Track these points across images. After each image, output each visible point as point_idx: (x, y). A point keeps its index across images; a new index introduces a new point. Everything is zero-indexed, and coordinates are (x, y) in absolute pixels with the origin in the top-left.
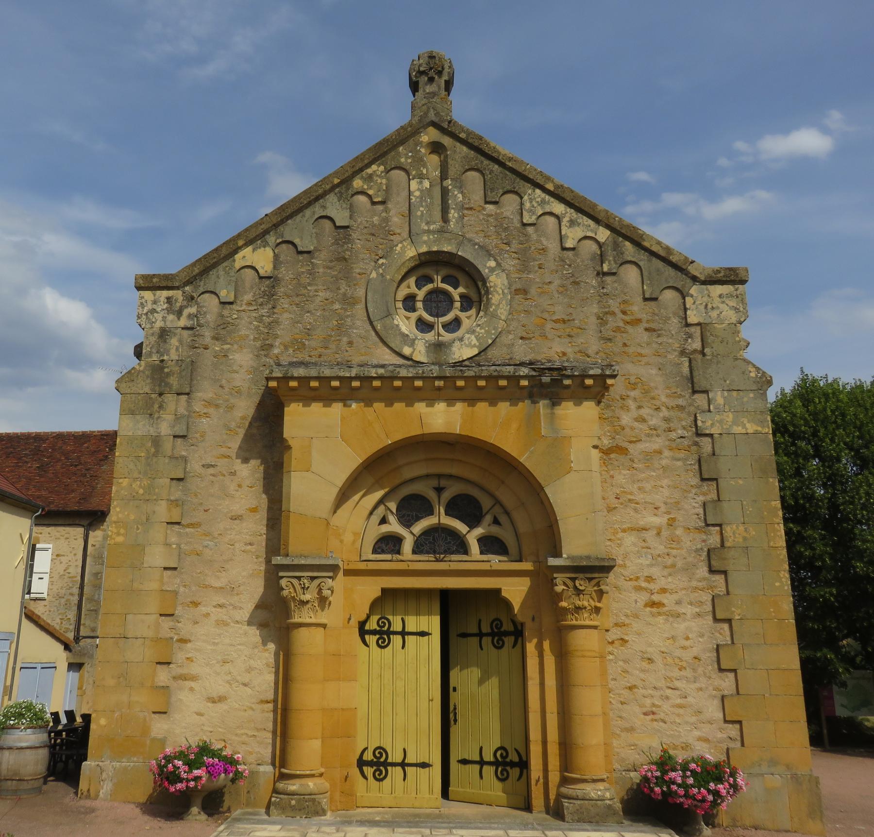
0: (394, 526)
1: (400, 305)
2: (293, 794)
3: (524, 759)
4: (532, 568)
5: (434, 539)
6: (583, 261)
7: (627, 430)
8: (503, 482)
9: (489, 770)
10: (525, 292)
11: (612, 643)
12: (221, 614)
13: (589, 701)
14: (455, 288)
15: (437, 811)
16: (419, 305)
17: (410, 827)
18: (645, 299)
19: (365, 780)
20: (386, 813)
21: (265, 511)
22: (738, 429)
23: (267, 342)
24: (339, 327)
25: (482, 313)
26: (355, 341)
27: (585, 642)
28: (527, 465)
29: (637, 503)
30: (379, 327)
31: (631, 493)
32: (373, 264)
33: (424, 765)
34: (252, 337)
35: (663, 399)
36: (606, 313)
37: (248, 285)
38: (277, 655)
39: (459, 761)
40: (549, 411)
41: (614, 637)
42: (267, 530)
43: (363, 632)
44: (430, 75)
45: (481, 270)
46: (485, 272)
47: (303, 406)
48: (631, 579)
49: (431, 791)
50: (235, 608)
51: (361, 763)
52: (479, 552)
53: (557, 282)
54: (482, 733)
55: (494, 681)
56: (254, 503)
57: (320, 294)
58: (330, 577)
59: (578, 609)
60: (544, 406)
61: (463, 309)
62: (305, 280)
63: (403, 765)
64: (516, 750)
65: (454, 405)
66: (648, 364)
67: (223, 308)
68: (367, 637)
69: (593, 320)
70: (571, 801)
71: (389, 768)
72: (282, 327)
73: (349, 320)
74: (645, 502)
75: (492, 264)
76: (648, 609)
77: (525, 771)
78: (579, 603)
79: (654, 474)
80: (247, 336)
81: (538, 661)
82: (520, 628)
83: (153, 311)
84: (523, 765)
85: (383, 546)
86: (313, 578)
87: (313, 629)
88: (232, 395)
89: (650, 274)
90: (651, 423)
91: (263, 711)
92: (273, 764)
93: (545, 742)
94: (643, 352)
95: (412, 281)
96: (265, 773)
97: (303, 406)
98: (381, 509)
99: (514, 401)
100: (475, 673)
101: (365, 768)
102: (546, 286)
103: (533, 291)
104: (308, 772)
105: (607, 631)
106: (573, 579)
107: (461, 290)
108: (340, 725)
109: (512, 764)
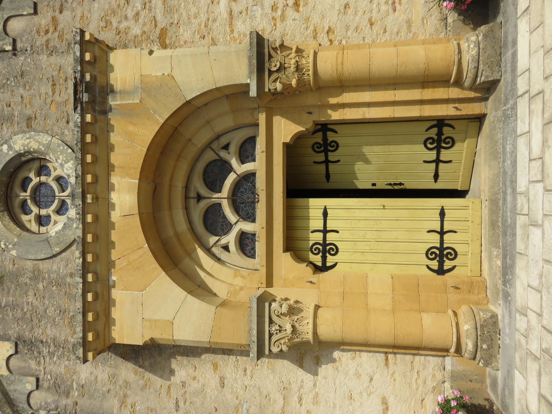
0: (231, 239)
1: (43, 229)
2: (476, 346)
3: (435, 123)
4: (264, 114)
5: (242, 203)
6: (4, 68)
7: (145, 29)
8: (190, 140)
9: (445, 155)
10: (29, 119)
11: (331, 41)
12: (308, 399)
13: (384, 58)
14: (31, 180)
15: (486, 204)
17: (514, 235)
18: (36, 12)
19: (456, 268)
20: (490, 253)
21: (216, 356)
23: (71, 349)
24: (58, 285)
25: (48, 158)
26: (70, 271)
27: (328, 64)
28: (166, 116)
29: (208, 19)
30: (57, 250)
31: (200, 25)
32: (6, 253)
33: (442, 214)
34: (67, 362)
36: (47, 47)
37: (23, 364)
38: (343, 351)
39: (436, 181)
40: (118, 95)
41: (326, 39)
42: (233, 355)
43: (324, 268)
45: (10, 158)
46: (12, 154)
47: (115, 325)
48: (275, 25)
49: (466, 208)
50: (302, 387)
51: (441, 271)
52: (253, 163)
53: (21, 91)
54: (410, 161)
55: (366, 150)
56: (209, 366)
57: (30, 300)
58: (270, 305)
59: (298, 68)
60: (115, 101)
61: (48, 174)
62: (19, 314)
63: (442, 233)
64: (426, 131)
65: (113, 185)
66: (90, 11)
67: (42, 387)
68: (328, 264)
69: (53, 59)
70: (479, 74)
71: (445, 246)
72: (58, 336)
73: (52, 276)
74: (207, 12)
75: (5, 147)
76: (301, 9)
77: (446, 122)
78: (293, 69)
79: (183, 4)
80: (66, 366)
81: (348, 107)
82: (319, 127)
84: (440, 123)
85: (248, 248)
86: (271, 322)
87: (319, 321)
88: (115, 383)
89: (14, 9)
90: (139, 8)
91: (395, 363)
92: (444, 356)
93: (422, 102)
94: (79, 15)
95: (25, 218)
96: (452, 365)
97: (115, 325)
98: (215, 250)
99: (108, 129)
100: (359, 167)
101: (445, 268)
102: (25, 101)
103: (28, 112)
104: (455, 330)
105: (320, 45)
106: (271, 73)
107: (32, 175)
108: (408, 293)
109: (440, 133)
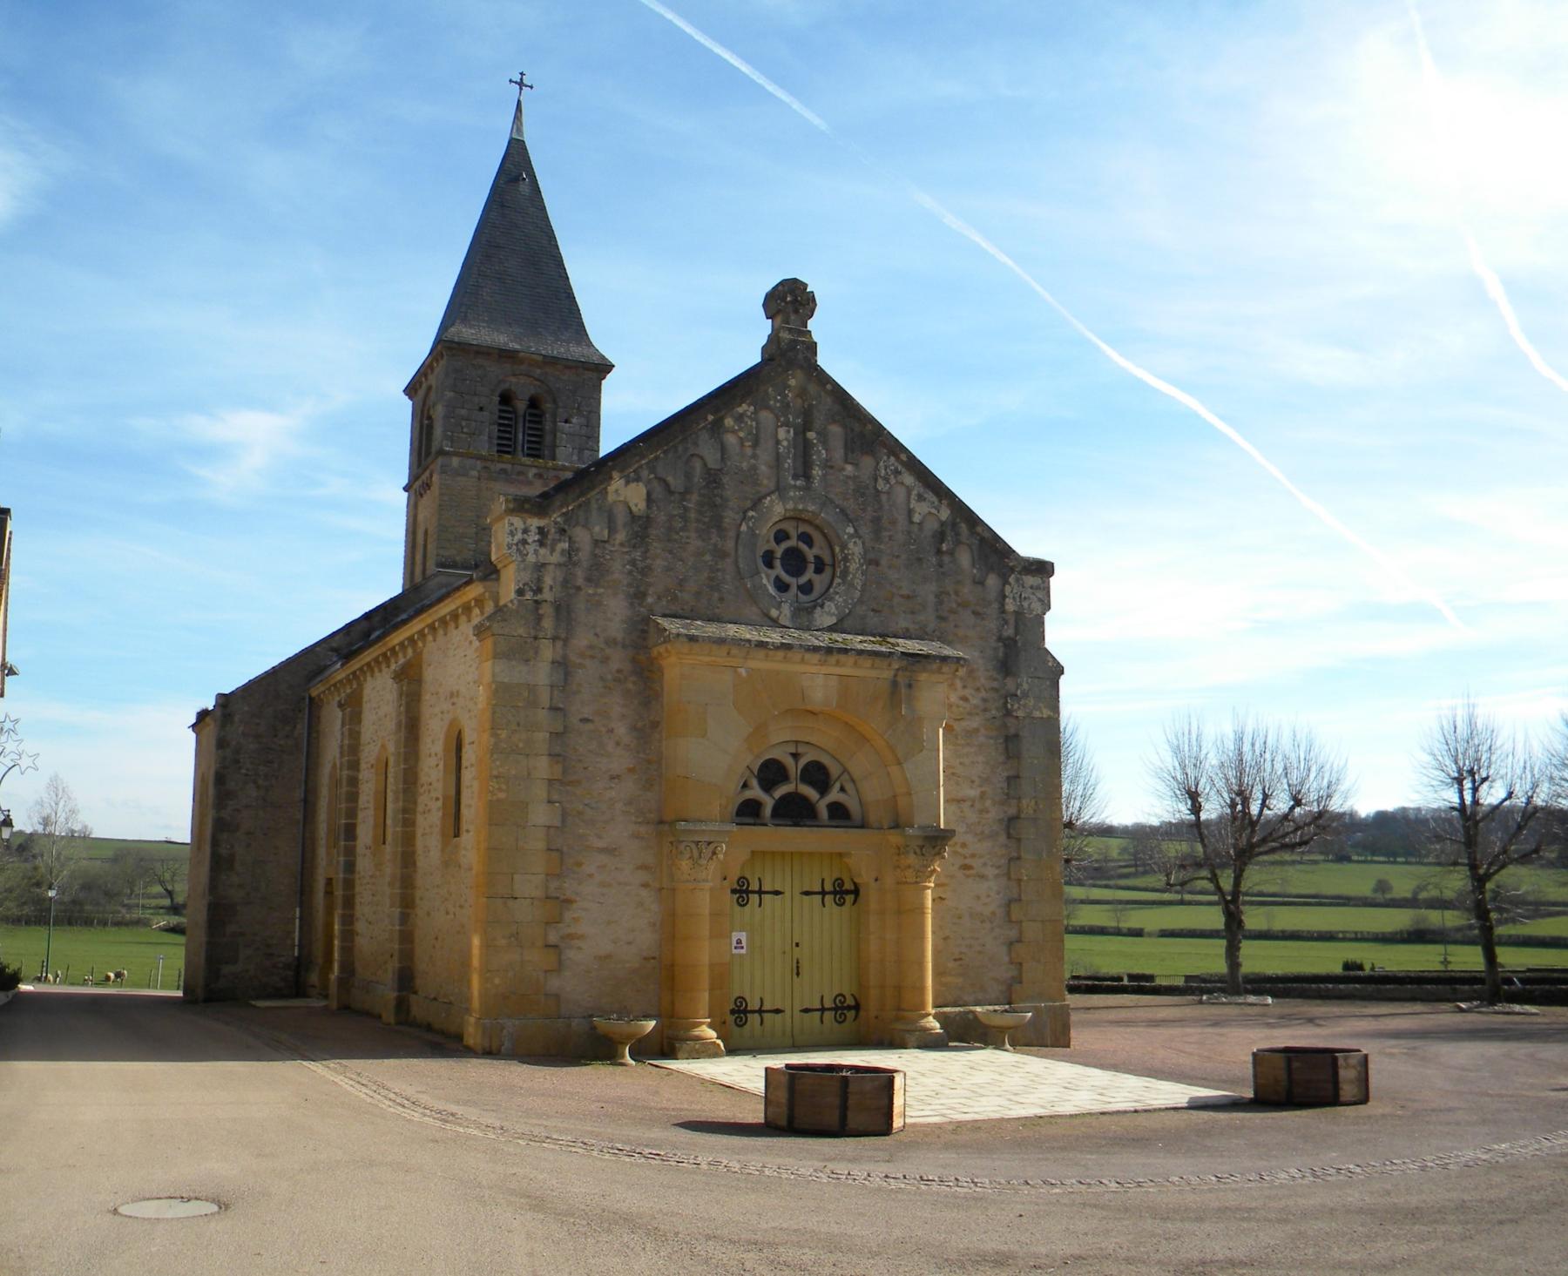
16: (778, 563)
22: (1037, 714)
35: (983, 680)
44: (790, 302)
63: (760, 1011)
83: (524, 542)
103: (884, 562)
